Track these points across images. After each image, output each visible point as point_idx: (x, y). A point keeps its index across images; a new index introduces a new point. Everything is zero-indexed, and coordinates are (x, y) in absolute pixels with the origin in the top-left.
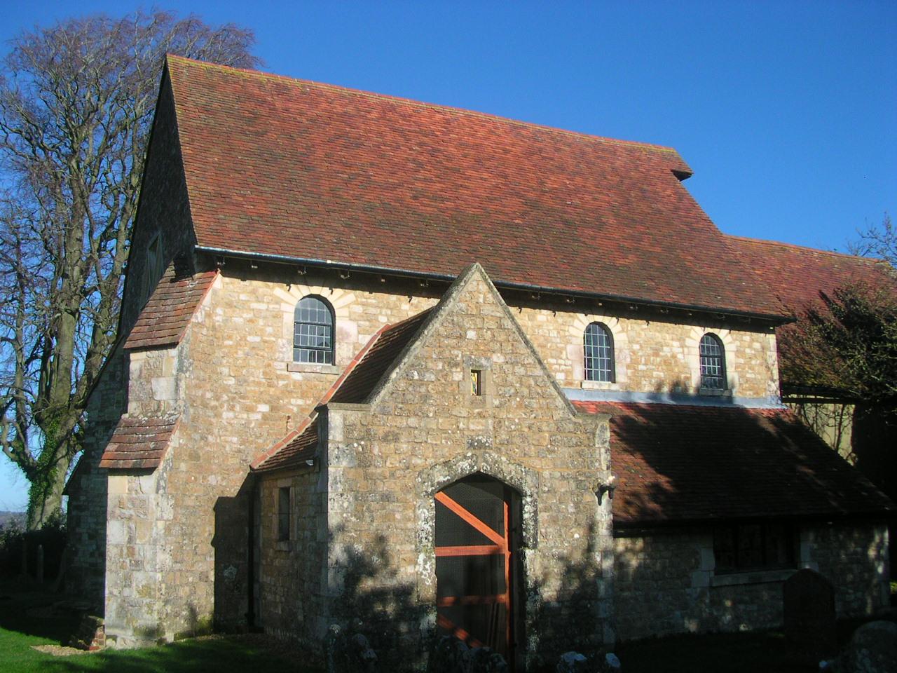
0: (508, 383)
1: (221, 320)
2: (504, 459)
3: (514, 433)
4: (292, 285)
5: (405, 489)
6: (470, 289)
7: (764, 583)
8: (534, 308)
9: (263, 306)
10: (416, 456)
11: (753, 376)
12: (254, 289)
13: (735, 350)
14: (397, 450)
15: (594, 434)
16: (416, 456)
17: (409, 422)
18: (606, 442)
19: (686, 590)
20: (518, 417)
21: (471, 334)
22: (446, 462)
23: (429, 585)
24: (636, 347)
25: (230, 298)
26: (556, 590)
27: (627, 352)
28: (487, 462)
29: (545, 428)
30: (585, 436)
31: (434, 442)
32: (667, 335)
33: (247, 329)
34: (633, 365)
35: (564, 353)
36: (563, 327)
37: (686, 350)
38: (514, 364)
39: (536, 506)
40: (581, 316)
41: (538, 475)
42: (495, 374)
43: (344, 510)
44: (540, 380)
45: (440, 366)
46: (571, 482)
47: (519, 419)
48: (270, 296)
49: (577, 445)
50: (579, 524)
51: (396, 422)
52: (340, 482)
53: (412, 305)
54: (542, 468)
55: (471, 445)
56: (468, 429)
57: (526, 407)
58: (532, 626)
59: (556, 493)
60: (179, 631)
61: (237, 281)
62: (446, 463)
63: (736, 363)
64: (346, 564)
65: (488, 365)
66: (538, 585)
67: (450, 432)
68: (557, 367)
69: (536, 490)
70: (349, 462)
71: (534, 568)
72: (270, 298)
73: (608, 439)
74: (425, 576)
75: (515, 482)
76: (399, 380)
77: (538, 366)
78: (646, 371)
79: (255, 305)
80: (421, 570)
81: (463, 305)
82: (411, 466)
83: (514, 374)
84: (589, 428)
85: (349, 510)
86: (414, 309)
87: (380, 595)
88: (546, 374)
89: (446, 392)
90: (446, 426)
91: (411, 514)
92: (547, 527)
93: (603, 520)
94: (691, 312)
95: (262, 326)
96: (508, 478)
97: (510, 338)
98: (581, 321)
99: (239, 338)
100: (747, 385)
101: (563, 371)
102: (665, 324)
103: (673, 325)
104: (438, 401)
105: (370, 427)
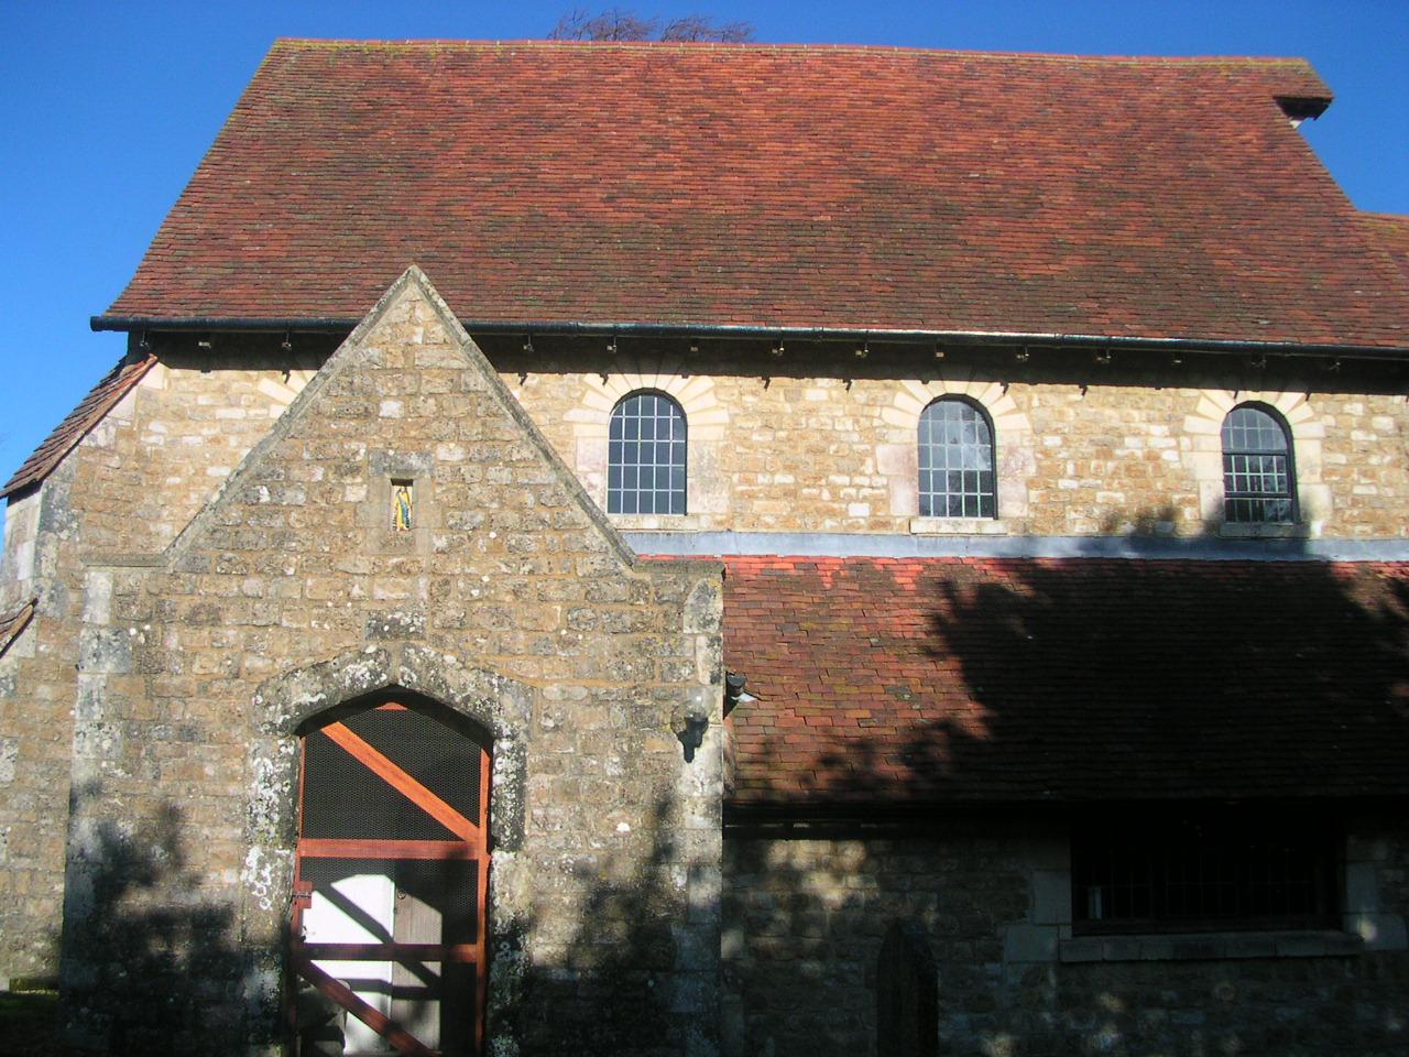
0: (471, 503)
1: (161, 443)
2: (450, 658)
3: (479, 604)
4: (292, 372)
5: (232, 718)
6: (393, 320)
7: (1226, 960)
8: (799, 376)
9: (238, 413)
10: (255, 652)
11: (1373, 491)
12: (223, 385)
13: (1323, 434)
14: (214, 641)
15: (680, 605)
16: (255, 652)
17: (244, 587)
18: (712, 621)
19: (988, 966)
20: (492, 571)
21: (391, 408)
22: (318, 665)
23: (267, 912)
24: (1052, 441)
25: (181, 403)
26: (566, 943)
27: (1029, 453)
28: (407, 663)
29: (553, 593)
30: (657, 609)
31: (295, 626)
32: (1135, 414)
33: (207, 455)
34: (1044, 478)
35: (869, 462)
36: (866, 410)
37: (1185, 441)
38: (485, 463)
39: (523, 760)
40: (913, 385)
41: (529, 691)
42: (441, 484)
43: (102, 755)
44: (549, 492)
45: (319, 473)
46: (616, 709)
47: (493, 576)
48: (253, 394)
49: (633, 629)
50: (631, 802)
51: (217, 586)
52: (99, 701)
53: (526, 388)
54: (542, 678)
55: (376, 631)
56: (372, 597)
57: (511, 549)
58: (504, 1014)
59: (575, 731)
60: (22, 975)
61: (195, 374)
62: (317, 667)
63: (1324, 465)
64: (100, 857)
65: (425, 467)
66: (519, 929)
67: (330, 604)
68: (853, 491)
69: (525, 726)
70: (118, 665)
71: (511, 892)
72: (252, 398)
73: (717, 617)
74: (260, 891)
75: (476, 707)
76: (229, 504)
77: (544, 462)
78: (1078, 492)
79: (222, 413)
80: (251, 879)
81: (374, 352)
82: (244, 673)
83: (484, 481)
84: (667, 592)
85: (113, 754)
86: (530, 397)
87: (162, 923)
88: (562, 481)
89: (328, 525)
90: (322, 594)
91: (237, 767)
92: (548, 806)
93: (695, 794)
94: (1178, 356)
95: (235, 448)
96: (458, 699)
97: (480, 411)
98: (911, 395)
99: (192, 471)
100: (1356, 512)
101: (865, 499)
102: (1130, 389)
103: (1152, 390)
104: (309, 543)
105: (164, 597)
